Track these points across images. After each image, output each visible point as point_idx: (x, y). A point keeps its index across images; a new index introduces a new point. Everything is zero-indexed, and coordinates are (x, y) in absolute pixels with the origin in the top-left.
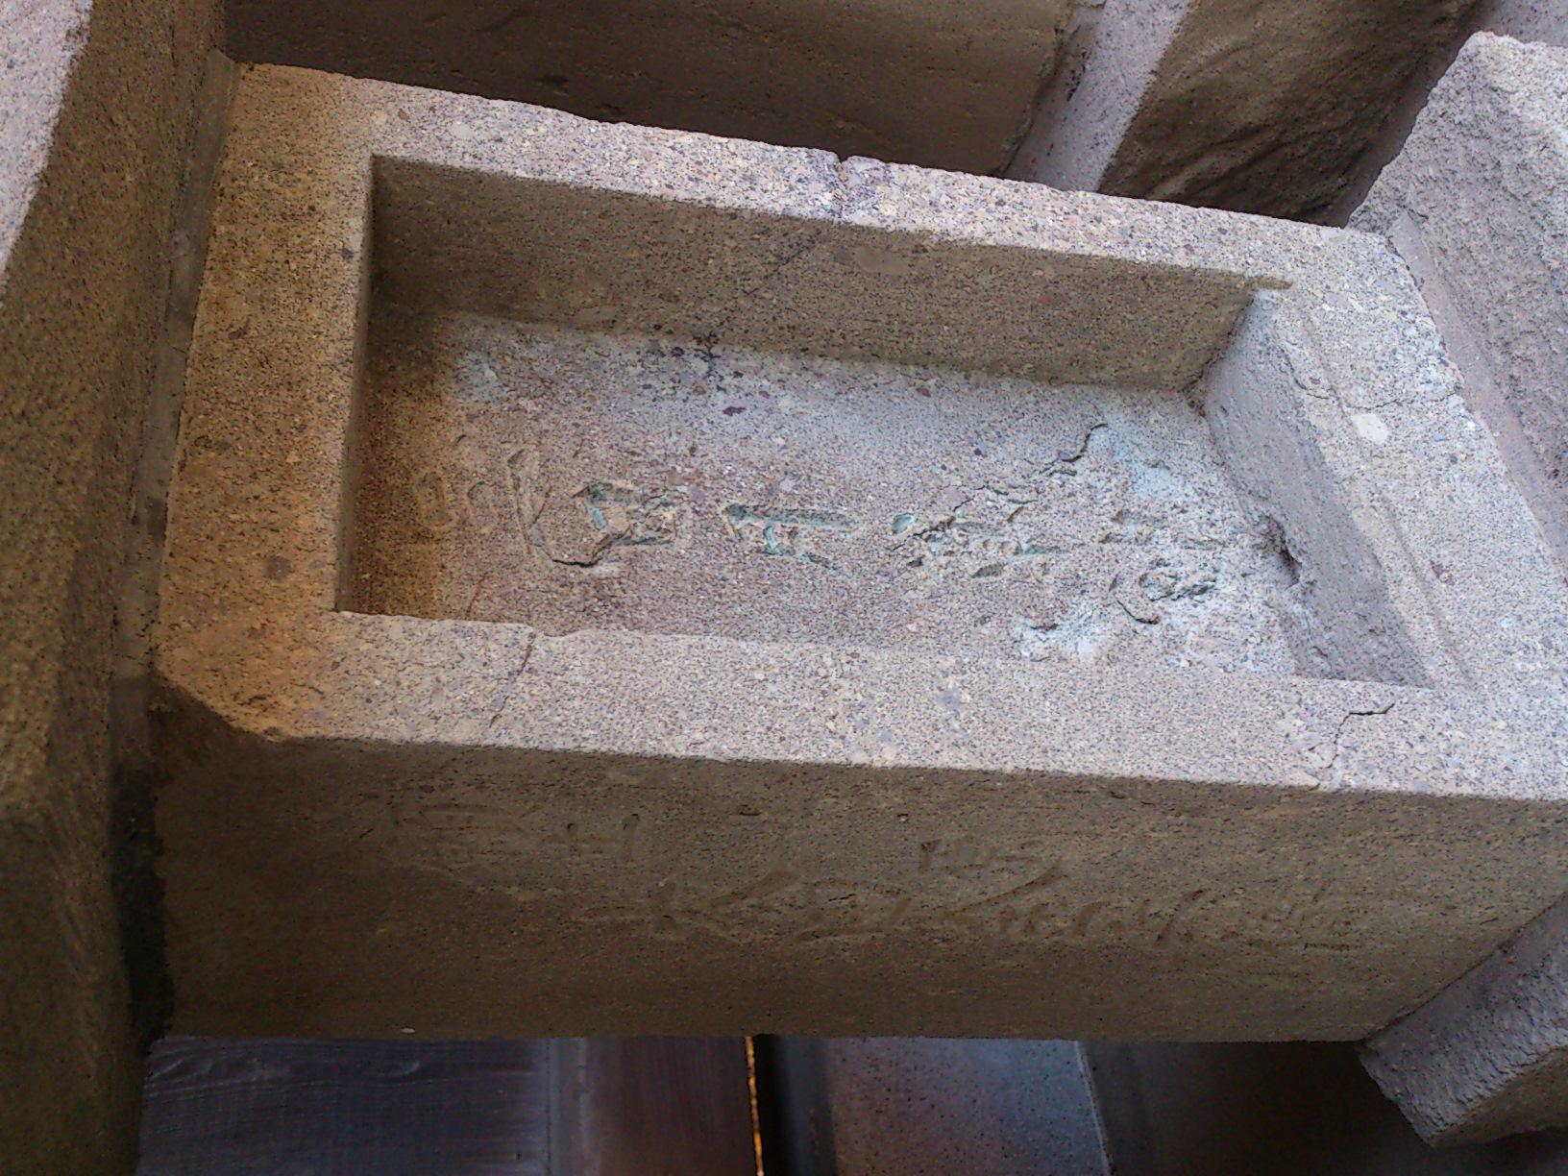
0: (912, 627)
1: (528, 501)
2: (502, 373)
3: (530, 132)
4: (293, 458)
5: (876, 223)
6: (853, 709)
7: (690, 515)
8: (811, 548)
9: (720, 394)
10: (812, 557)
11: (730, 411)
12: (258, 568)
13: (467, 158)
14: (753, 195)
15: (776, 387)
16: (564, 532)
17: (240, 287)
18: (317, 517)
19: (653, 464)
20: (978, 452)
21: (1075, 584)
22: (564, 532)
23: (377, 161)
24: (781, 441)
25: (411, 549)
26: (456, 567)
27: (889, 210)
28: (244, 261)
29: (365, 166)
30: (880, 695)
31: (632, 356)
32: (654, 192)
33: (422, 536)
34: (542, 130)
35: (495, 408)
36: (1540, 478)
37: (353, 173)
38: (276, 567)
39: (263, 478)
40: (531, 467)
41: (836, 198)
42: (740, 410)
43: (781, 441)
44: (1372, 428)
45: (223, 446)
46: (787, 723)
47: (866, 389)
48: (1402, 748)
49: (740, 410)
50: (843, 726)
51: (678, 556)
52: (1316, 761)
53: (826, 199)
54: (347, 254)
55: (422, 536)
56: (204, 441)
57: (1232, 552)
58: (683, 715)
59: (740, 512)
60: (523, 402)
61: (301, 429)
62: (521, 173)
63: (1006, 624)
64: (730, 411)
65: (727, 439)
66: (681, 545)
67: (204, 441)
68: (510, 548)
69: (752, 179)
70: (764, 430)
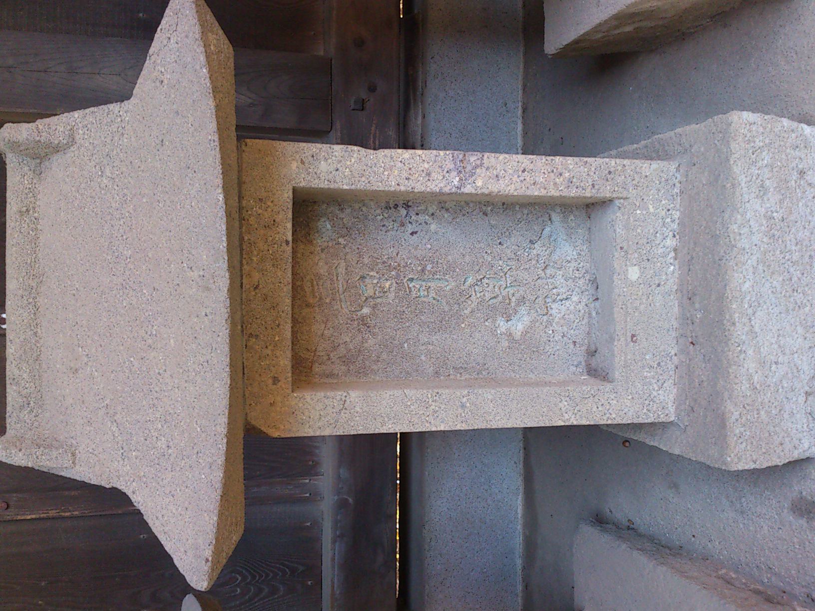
0: (463, 325)
1: (341, 286)
2: (333, 226)
3: (348, 163)
4: (277, 338)
5: (474, 191)
6: (435, 412)
7: (395, 285)
8: (434, 295)
9: (409, 225)
10: (434, 299)
11: (412, 234)
12: (270, 381)
13: (326, 182)
14: (429, 184)
15: (430, 219)
16: (353, 298)
17: (255, 265)
18: (285, 361)
19: (384, 263)
20: (500, 243)
21: (522, 301)
22: (353, 298)
23: (295, 190)
24: (429, 246)
25: (306, 311)
26: (318, 317)
27: (479, 183)
28: (255, 253)
29: (291, 194)
30: (443, 407)
31: (378, 211)
32: (393, 189)
33: (308, 305)
34: (353, 160)
35: (330, 244)
36: (685, 297)
37: (288, 195)
38: (276, 380)
39: (270, 347)
40: (343, 264)
41: (461, 179)
42: (416, 233)
43: (429, 246)
44: (634, 273)
45: (257, 336)
46: (415, 419)
47: (464, 215)
48: (595, 409)
49: (416, 233)
50: (431, 419)
51: (389, 303)
52: (566, 416)
53: (456, 181)
54: (287, 242)
55: (308, 305)
56: (251, 335)
57: (581, 282)
58: (386, 419)
59: (412, 280)
60: (340, 240)
61: (278, 326)
62: (345, 187)
63: (494, 321)
64: (412, 234)
65: (410, 248)
66: (392, 295)
67: (251, 335)
68: (335, 307)
69: (429, 174)
70: (424, 241)
